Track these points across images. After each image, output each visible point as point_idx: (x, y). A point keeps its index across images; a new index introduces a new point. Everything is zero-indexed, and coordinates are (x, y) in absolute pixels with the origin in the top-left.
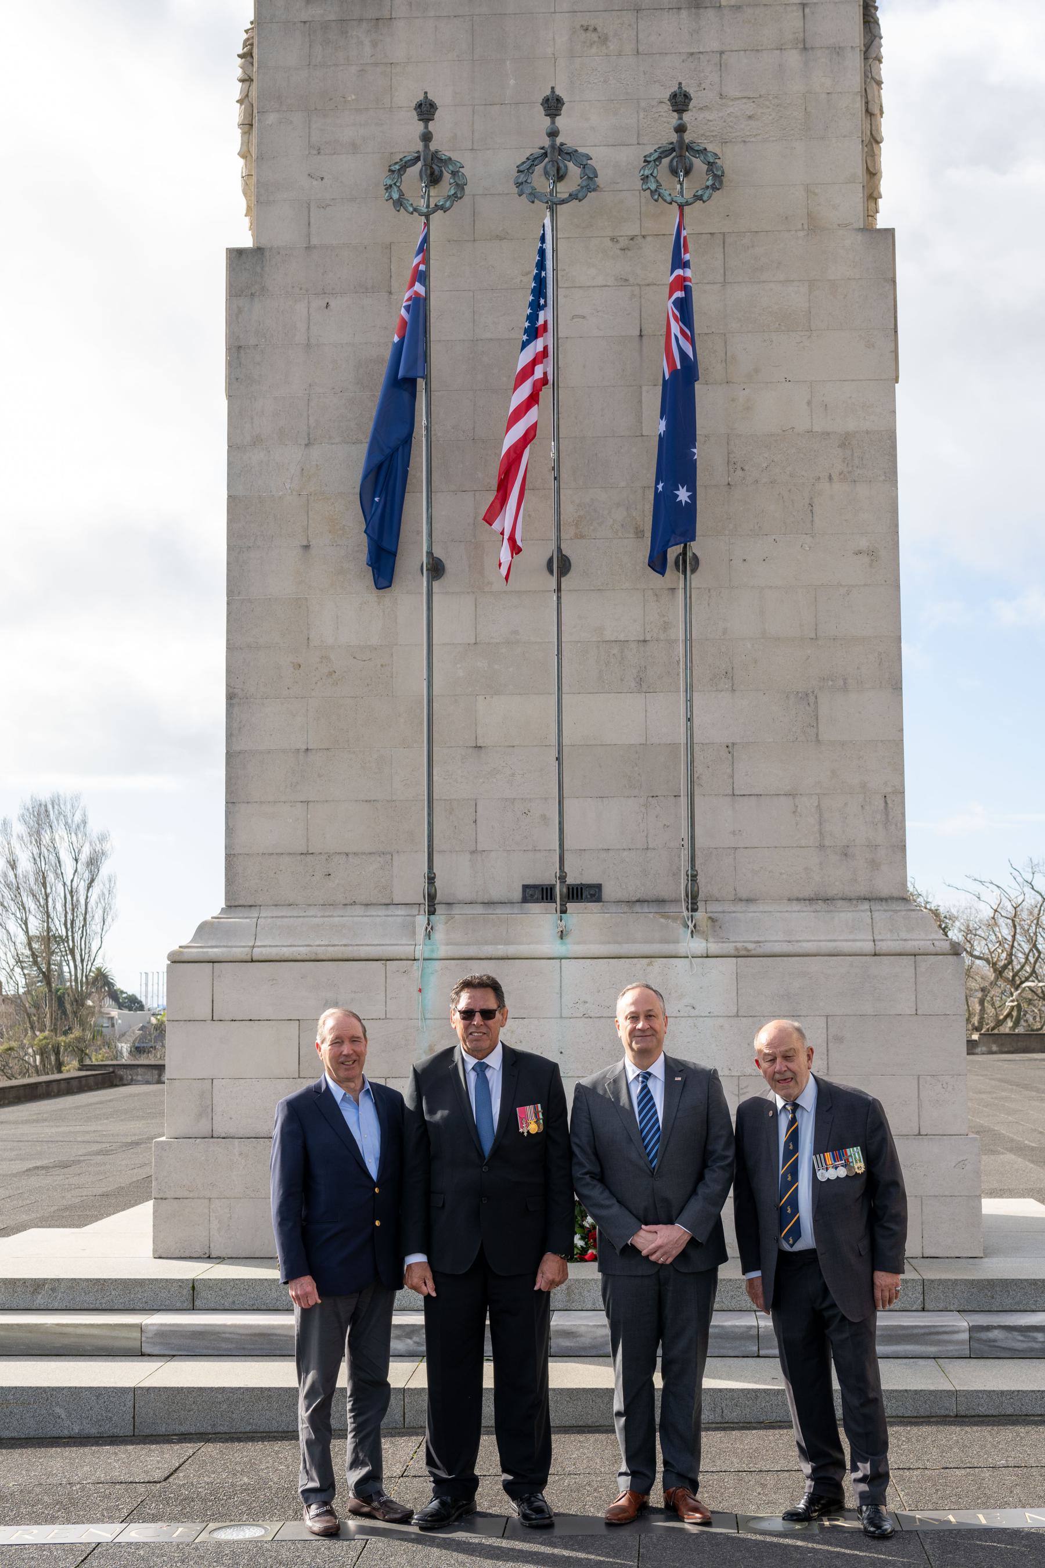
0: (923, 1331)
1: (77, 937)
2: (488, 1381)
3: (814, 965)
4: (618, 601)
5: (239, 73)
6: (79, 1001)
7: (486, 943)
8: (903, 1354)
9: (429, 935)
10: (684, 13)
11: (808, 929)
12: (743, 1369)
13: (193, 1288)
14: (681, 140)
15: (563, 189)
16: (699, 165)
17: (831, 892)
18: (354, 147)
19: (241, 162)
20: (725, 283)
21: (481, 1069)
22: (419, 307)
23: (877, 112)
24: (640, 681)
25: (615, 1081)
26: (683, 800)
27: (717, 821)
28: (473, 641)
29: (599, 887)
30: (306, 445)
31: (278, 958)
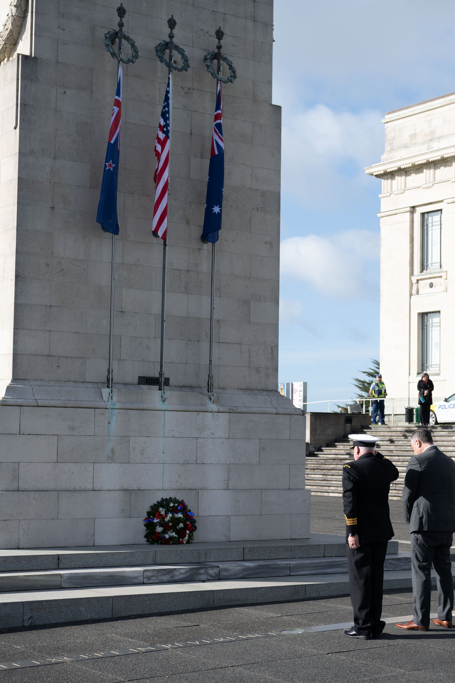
0: (341, 563)
4: (185, 253)
8: (335, 572)
13: (58, 559)
24: (186, 288)
28: (122, 262)
30: (54, 159)
31: (49, 405)
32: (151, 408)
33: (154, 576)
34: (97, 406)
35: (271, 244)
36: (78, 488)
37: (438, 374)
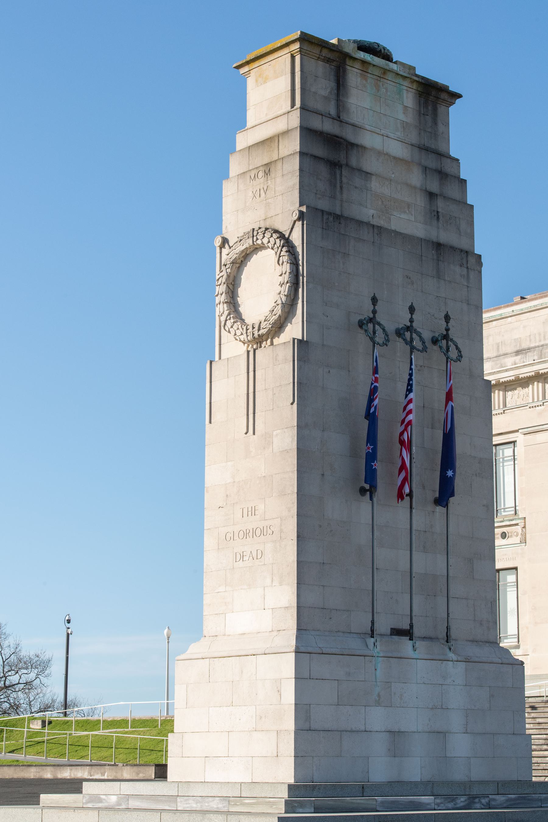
24: (424, 547)
32: (406, 657)
33: (442, 803)
36: (354, 729)
37: (518, 647)
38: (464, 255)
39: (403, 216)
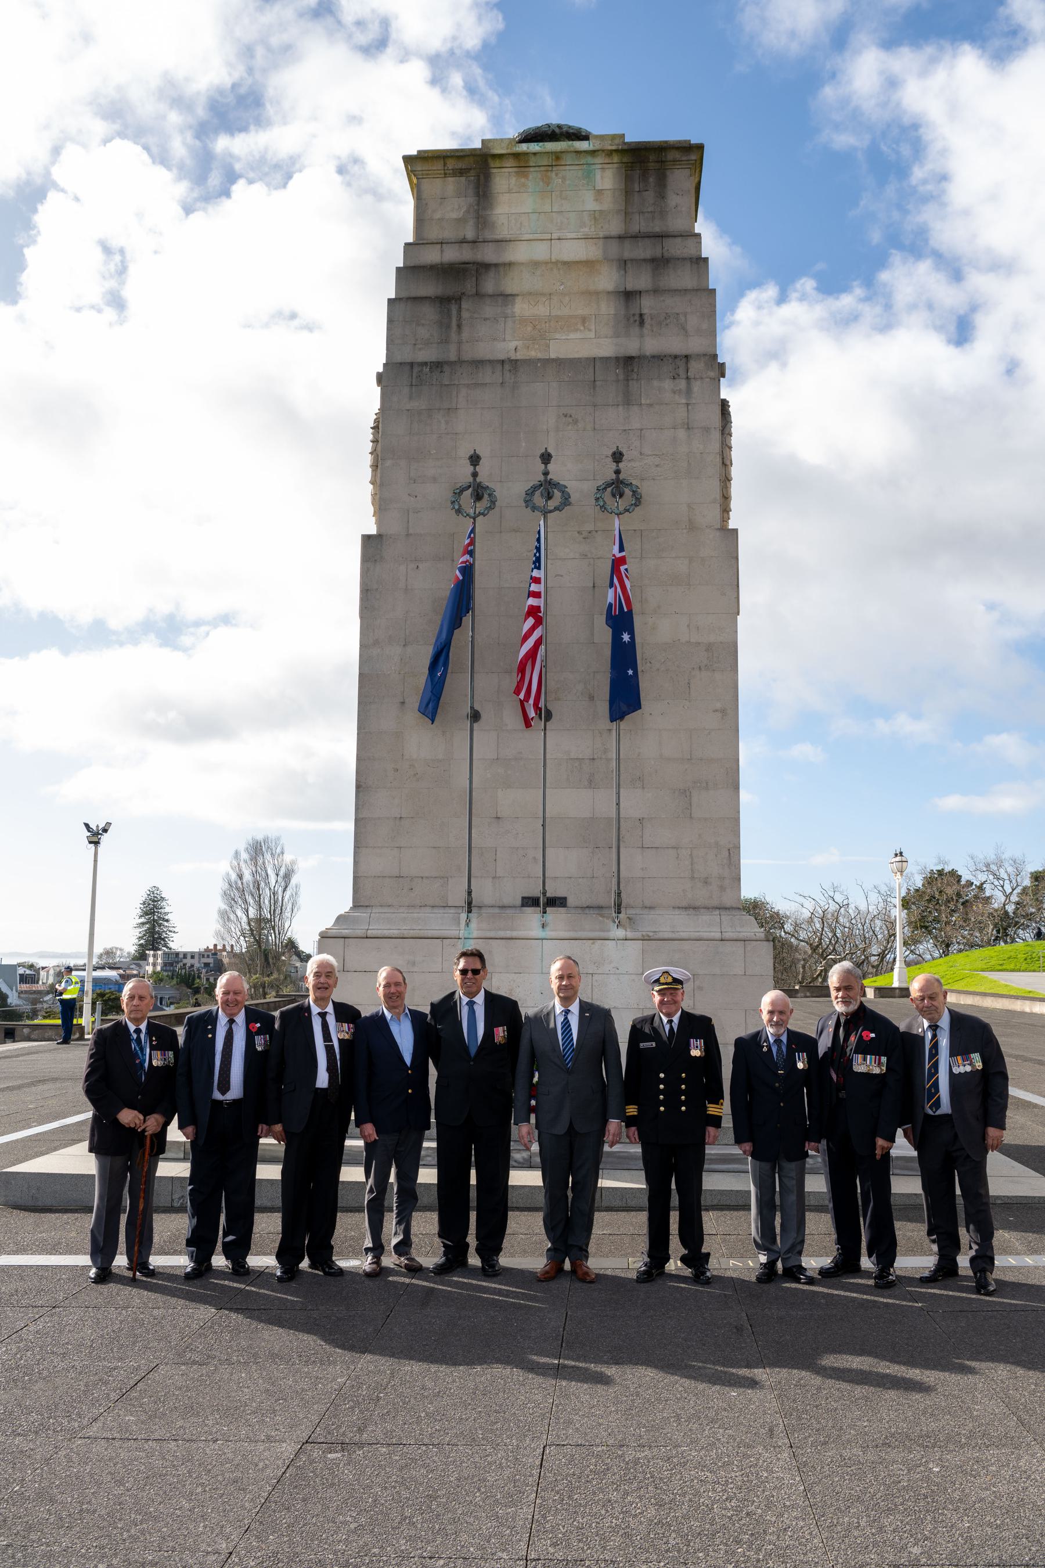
1: (277, 920)
2: (473, 1181)
3: (686, 945)
5: (371, 437)
6: (277, 957)
7: (500, 929)
9: (467, 925)
10: (621, 408)
11: (684, 925)
12: (622, 1179)
14: (618, 478)
15: (552, 504)
16: (628, 492)
17: (698, 904)
18: (434, 480)
19: (371, 486)
20: (642, 558)
21: (471, 1004)
22: (468, 571)
23: (728, 463)
24: (590, 781)
25: (548, 1014)
26: (614, 850)
27: (633, 863)
29: (565, 899)
34: (445, 936)
35: (723, 711)
38: (681, 363)
39: (572, 336)
